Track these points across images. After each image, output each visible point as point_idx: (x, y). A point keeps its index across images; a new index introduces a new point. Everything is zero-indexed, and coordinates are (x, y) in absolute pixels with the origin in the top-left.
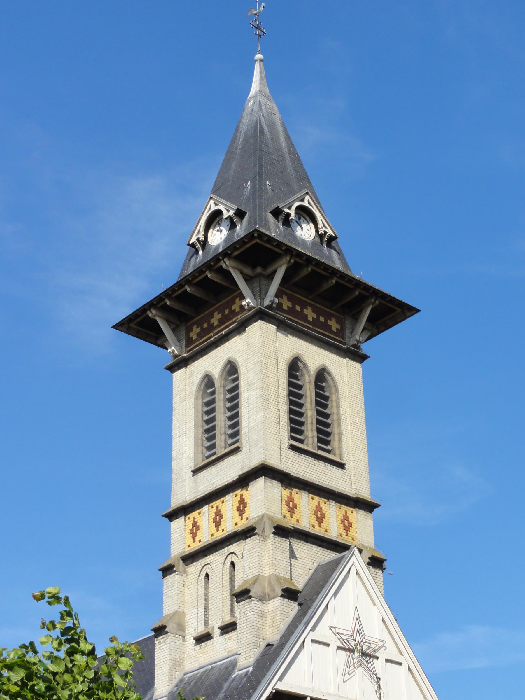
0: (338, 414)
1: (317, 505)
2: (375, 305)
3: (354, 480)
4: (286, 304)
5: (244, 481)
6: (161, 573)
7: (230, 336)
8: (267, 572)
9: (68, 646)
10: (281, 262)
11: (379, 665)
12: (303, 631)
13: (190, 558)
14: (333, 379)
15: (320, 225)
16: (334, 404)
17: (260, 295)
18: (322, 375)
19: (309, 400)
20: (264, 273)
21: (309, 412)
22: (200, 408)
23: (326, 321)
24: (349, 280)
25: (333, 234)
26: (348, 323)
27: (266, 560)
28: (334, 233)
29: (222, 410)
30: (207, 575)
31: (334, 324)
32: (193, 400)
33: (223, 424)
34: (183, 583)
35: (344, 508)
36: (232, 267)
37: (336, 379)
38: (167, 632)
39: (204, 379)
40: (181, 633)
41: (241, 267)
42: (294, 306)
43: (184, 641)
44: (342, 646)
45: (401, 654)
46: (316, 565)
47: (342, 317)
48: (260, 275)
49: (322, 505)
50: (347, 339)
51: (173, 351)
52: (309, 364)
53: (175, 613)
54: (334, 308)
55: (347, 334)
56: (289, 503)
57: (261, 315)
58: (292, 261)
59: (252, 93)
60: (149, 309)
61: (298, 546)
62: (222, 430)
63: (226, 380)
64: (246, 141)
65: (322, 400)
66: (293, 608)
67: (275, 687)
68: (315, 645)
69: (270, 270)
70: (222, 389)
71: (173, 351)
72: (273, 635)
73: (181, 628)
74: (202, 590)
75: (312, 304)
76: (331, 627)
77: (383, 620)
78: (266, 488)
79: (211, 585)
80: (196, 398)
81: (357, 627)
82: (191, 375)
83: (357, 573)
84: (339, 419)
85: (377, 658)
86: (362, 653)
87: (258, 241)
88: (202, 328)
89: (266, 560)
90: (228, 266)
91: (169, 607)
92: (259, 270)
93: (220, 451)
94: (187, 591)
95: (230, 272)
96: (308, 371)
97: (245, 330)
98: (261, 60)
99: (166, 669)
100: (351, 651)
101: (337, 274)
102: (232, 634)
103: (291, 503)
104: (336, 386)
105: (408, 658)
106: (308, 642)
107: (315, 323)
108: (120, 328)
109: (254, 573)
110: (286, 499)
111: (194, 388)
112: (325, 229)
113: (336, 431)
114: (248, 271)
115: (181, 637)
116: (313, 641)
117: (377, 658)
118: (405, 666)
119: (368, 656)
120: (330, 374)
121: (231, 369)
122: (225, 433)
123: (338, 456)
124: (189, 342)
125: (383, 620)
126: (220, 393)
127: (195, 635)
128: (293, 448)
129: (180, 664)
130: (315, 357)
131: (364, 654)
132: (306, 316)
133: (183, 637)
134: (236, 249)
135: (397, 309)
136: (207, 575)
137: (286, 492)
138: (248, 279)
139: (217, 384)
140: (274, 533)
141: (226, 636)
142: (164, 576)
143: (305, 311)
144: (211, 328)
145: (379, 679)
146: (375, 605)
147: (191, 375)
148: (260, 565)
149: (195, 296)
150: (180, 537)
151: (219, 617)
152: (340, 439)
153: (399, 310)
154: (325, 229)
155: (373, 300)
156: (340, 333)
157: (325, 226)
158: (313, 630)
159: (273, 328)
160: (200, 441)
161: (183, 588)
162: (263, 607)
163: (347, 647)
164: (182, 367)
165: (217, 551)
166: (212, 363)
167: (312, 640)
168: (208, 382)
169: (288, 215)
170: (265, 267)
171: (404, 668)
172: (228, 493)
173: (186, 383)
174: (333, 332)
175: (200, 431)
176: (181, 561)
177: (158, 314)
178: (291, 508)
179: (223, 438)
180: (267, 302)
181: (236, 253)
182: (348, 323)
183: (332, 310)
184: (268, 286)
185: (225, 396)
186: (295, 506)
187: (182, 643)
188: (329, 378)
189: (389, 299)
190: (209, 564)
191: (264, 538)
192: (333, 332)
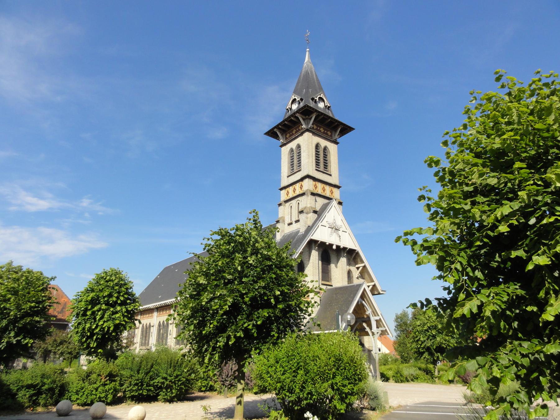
3: (334, 180)
4: (315, 127)
5: (302, 179)
8: (309, 206)
13: (286, 202)
18: (325, 148)
21: (322, 159)
27: (308, 202)
31: (329, 133)
59: (306, 61)
65: (325, 156)
73: (284, 221)
91: (280, 215)
93: (295, 171)
100: (332, 228)
105: (349, 231)
107: (324, 133)
114: (304, 117)
121: (299, 146)
130: (324, 143)
131: (336, 229)
137: (314, 183)
138: (304, 120)
150: (284, 195)
159: (311, 134)
166: (293, 145)
168: (292, 150)
173: (285, 150)
191: (308, 196)
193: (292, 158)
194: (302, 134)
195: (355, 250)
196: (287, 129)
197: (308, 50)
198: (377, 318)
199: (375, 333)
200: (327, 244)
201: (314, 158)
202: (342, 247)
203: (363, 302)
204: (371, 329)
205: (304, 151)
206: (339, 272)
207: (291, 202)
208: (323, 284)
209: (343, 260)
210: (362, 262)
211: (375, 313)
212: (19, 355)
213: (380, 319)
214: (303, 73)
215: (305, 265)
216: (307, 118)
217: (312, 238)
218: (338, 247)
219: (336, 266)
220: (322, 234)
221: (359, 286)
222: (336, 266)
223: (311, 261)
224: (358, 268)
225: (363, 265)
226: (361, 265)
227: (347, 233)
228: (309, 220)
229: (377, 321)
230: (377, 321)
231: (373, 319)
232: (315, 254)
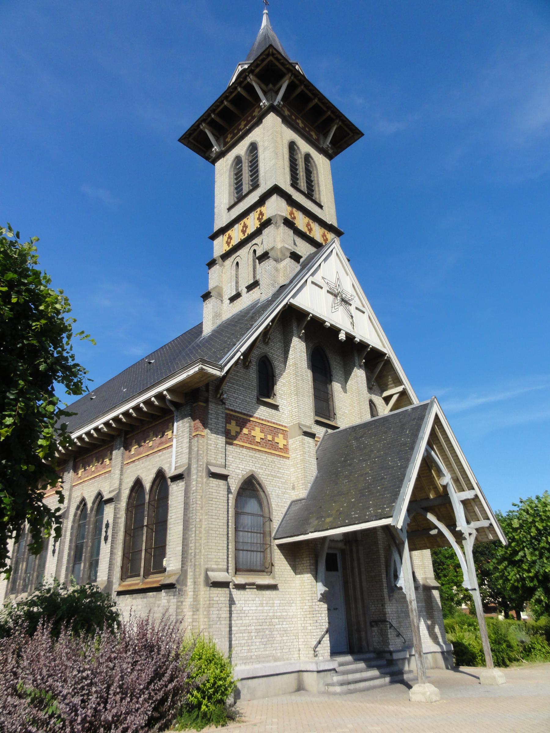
0: (318, 180)
3: (329, 214)
5: (262, 201)
6: (202, 299)
8: (279, 246)
9: (124, 716)
10: (285, 78)
11: (352, 309)
12: (306, 274)
13: (225, 256)
14: (314, 162)
16: (315, 176)
18: (308, 157)
19: (301, 167)
21: (301, 173)
22: (232, 176)
27: (278, 239)
29: (247, 171)
30: (237, 263)
32: (228, 173)
33: (247, 179)
38: (211, 296)
39: (234, 160)
40: (221, 299)
41: (259, 82)
43: (222, 303)
46: (308, 254)
48: (271, 90)
49: (311, 223)
51: (216, 149)
53: (217, 287)
55: (321, 142)
57: (272, 108)
59: (262, 27)
60: (201, 124)
62: (247, 182)
63: (249, 156)
64: (259, 43)
65: (309, 173)
66: (297, 267)
69: (278, 86)
70: (247, 161)
71: (216, 149)
72: (283, 281)
73: (220, 296)
74: (234, 272)
76: (323, 278)
77: (353, 285)
78: (277, 200)
79: (240, 270)
80: (230, 171)
81: (338, 283)
82: (227, 160)
83: (337, 254)
84: (318, 183)
85: (351, 305)
89: (278, 239)
91: (212, 284)
93: (245, 192)
94: (224, 275)
96: (301, 153)
97: (262, 122)
98: (267, 14)
99: (210, 317)
100: (336, 296)
102: (256, 290)
104: (316, 166)
105: (368, 309)
106: (309, 282)
109: (271, 246)
111: (229, 167)
113: (317, 189)
116: (313, 283)
117: (351, 305)
118: (366, 315)
119: (345, 302)
120: (312, 159)
121: (253, 147)
122: (249, 183)
124: (225, 144)
125: (353, 285)
126: (245, 163)
127: (230, 296)
130: (304, 147)
131: (343, 300)
133: (222, 301)
134: (258, 66)
136: (237, 263)
137: (289, 209)
138: (265, 93)
139: (243, 159)
140: (283, 223)
141: (251, 292)
142: (209, 269)
145: (352, 317)
146: (347, 275)
147: (227, 160)
148: (275, 241)
149: (230, 109)
150: (220, 246)
151: (246, 279)
152: (319, 194)
158: (313, 275)
159: (279, 120)
160: (232, 194)
164: (221, 158)
166: (241, 149)
168: (238, 160)
170: (274, 85)
171: (366, 316)
172: (251, 212)
173: (223, 169)
175: (233, 188)
176: (220, 259)
177: (207, 127)
179: (247, 186)
180: (276, 103)
182: (322, 138)
188: (312, 161)
191: (278, 227)
193: (238, 175)
194: (259, 122)
195: (383, 354)
196: (225, 122)
197: (265, 11)
198: (468, 495)
199: (466, 535)
201: (287, 156)
202: (357, 339)
203: (433, 453)
204: (451, 524)
205: (265, 149)
206: (353, 400)
207: (238, 253)
208: (318, 423)
209: (359, 376)
210: (398, 382)
211: (462, 481)
212: (527, 587)
213: (476, 496)
214: (256, 46)
215: (277, 371)
216: (271, 90)
217: (294, 302)
218: (350, 338)
219: (345, 390)
220: (313, 301)
221: (424, 409)
222: (345, 390)
223: (290, 362)
224: (387, 400)
225: (400, 389)
226: (394, 391)
227: (366, 315)
228: (281, 274)
229: (465, 503)
230: (465, 503)
231: (457, 498)
232: (298, 349)
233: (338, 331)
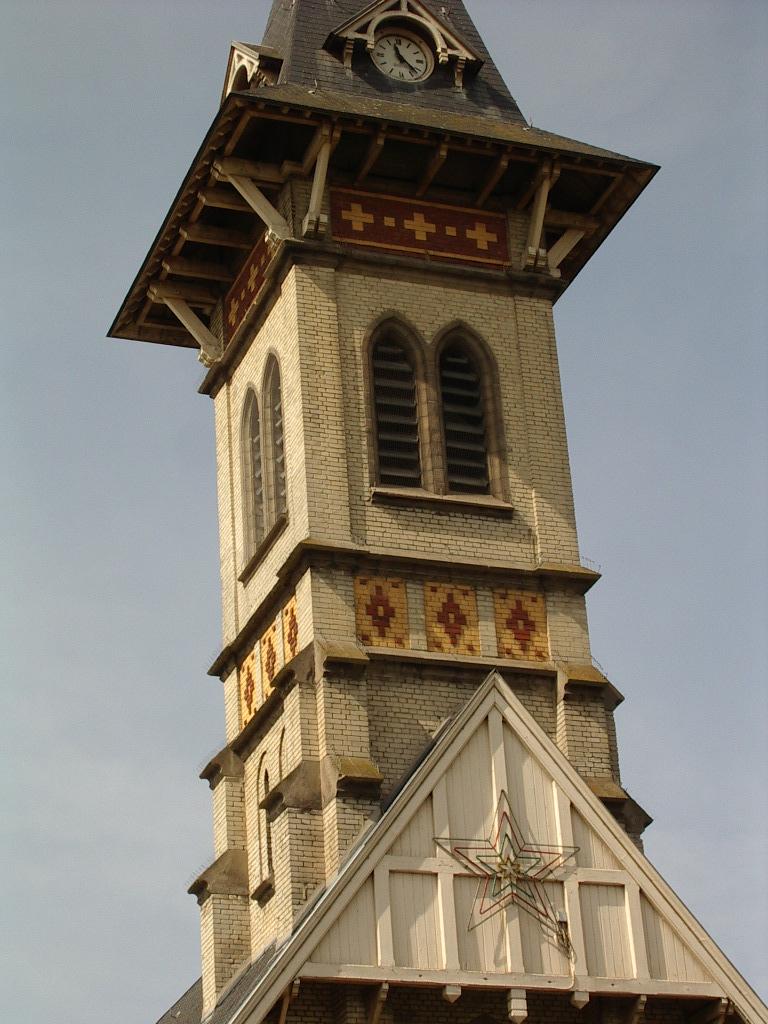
1: (445, 601)
2: (554, 180)
4: (358, 218)
7: (269, 303)
15: (440, 44)
17: (294, 217)
20: (299, 169)
23: (461, 233)
24: (474, 141)
25: (470, 57)
26: (515, 225)
28: (474, 55)
31: (481, 236)
34: (239, 794)
35: (514, 595)
36: (232, 175)
37: (490, 343)
40: (240, 890)
41: (251, 170)
42: (379, 221)
44: (466, 872)
45: (621, 867)
47: (502, 216)
48: (293, 176)
50: (513, 259)
52: (420, 327)
54: (480, 202)
56: (376, 610)
58: (337, 135)
61: (400, 690)
67: (301, 974)
68: (399, 880)
69: (308, 162)
75: (420, 206)
86: (518, 879)
87: (252, 113)
88: (379, 221)
90: (224, 176)
92: (287, 167)
95: (230, 184)
96: (419, 341)
101: (444, 136)
103: (381, 609)
108: (120, 334)
110: (369, 603)
112: (450, 52)
114: (268, 174)
115: (239, 898)
123: (500, 496)
128: (379, 500)
129: (242, 948)
130: (430, 308)
132: (412, 232)
134: (228, 136)
135: (612, 175)
137: (366, 592)
138: (272, 195)
143: (408, 225)
144: (251, 296)
153: (619, 177)
154: (450, 52)
155: (546, 170)
156: (500, 248)
157: (450, 46)
161: (241, 804)
162: (313, 823)
163: (478, 872)
165: (272, 725)
167: (391, 872)
169: (360, 45)
174: (480, 253)
178: (380, 618)
181: (230, 147)
183: (476, 208)
184: (309, 193)
185: (274, 424)
186: (390, 613)
187: (244, 908)
189: (579, 159)
190: (265, 753)
192: (480, 253)
200: (453, 993)
233: (502, 995)
